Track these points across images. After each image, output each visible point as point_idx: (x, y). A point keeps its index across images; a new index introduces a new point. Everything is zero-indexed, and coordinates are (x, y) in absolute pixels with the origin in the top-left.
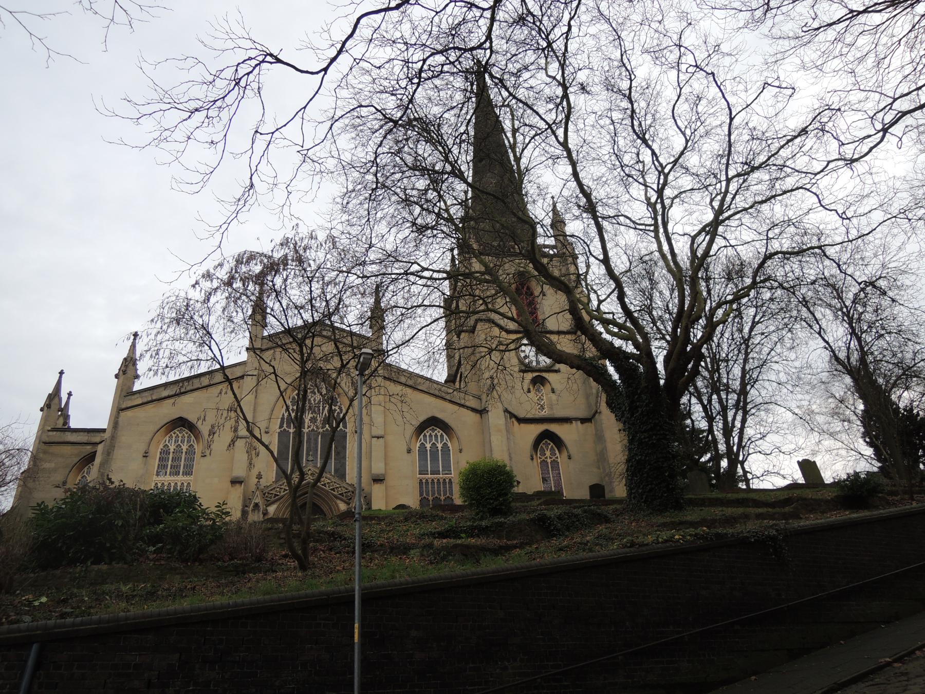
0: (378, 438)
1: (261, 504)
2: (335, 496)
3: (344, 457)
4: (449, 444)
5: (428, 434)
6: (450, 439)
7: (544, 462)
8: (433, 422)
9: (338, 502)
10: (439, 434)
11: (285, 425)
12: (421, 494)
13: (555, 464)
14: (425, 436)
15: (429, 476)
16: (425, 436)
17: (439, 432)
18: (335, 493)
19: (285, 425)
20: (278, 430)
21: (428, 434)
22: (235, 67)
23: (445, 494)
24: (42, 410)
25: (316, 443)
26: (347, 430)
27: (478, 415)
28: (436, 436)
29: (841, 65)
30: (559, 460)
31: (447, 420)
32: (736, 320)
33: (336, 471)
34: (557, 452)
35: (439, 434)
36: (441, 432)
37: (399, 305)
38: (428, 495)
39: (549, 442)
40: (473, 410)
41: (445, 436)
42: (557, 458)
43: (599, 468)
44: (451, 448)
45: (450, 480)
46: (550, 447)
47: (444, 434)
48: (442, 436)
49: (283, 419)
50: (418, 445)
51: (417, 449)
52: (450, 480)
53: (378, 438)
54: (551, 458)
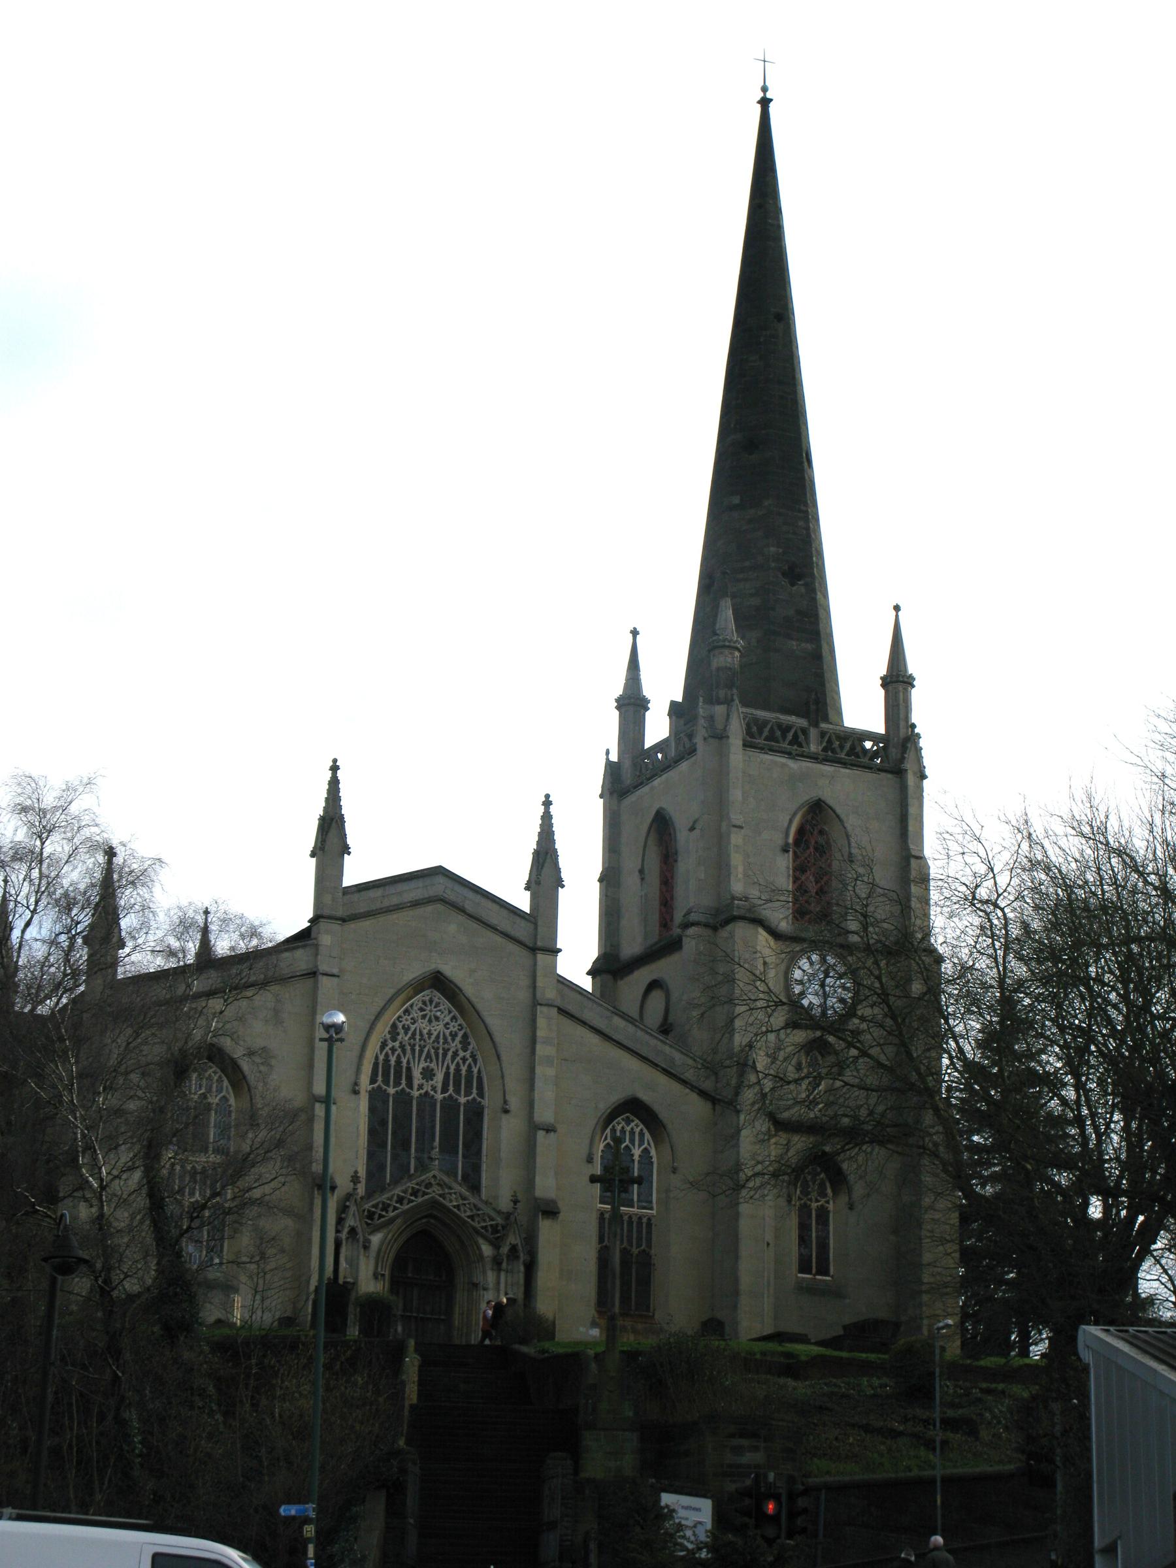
1: (359, 1230)
2: (477, 1232)
3: (479, 1152)
4: (653, 1152)
6: (836, 1193)
8: (633, 1107)
9: (481, 1241)
10: (637, 1130)
13: (823, 1215)
15: (635, 1210)
17: (637, 1126)
18: (475, 1224)
20: (370, 1088)
22: (995, 872)
23: (639, 1245)
27: (709, 1105)
28: (632, 1132)
30: (831, 1207)
31: (656, 1108)
34: (829, 1191)
35: (637, 1130)
36: (641, 1126)
38: (630, 1243)
39: (632, 1117)
41: (647, 1136)
44: (654, 1160)
45: (649, 1219)
47: (645, 1131)
48: (641, 1134)
51: (600, 1154)
52: (649, 1219)
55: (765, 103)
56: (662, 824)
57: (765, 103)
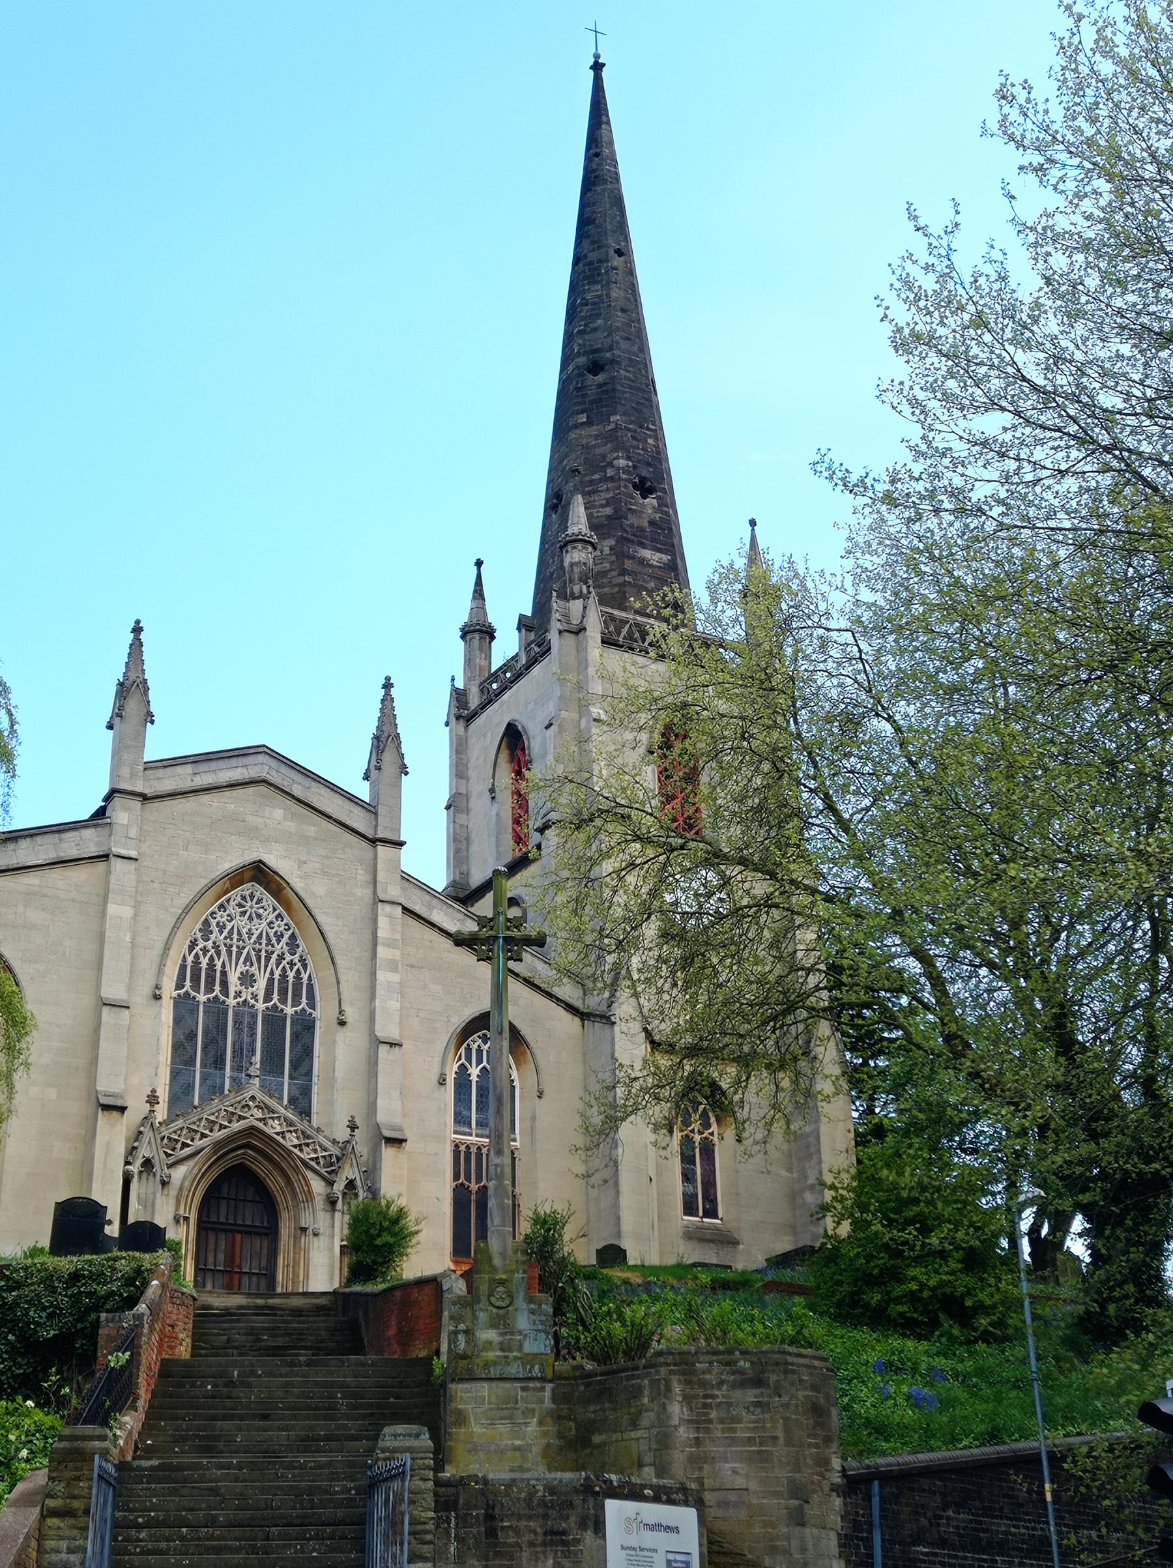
0: (392, 1045)
5: (474, 1047)
7: (687, 1141)
9: (310, 1175)
11: (188, 983)
12: (456, 1176)
13: (708, 1150)
14: (468, 1050)
16: (468, 1050)
19: (188, 983)
20: (175, 994)
21: (474, 1047)
24: (110, 727)
25: (253, 1034)
26: (317, 1014)
27: (577, 1020)
29: (965, 454)
32: (631, 879)
33: (292, 1101)
37: (136, 804)
38: (468, 1178)
40: (570, 1008)
42: (712, 1134)
43: (790, 1170)
46: (701, 1108)
49: (183, 968)
50: (455, 1068)
53: (392, 1045)
54: (700, 1133)
55: (597, 67)
56: (513, 737)
57: (597, 67)
